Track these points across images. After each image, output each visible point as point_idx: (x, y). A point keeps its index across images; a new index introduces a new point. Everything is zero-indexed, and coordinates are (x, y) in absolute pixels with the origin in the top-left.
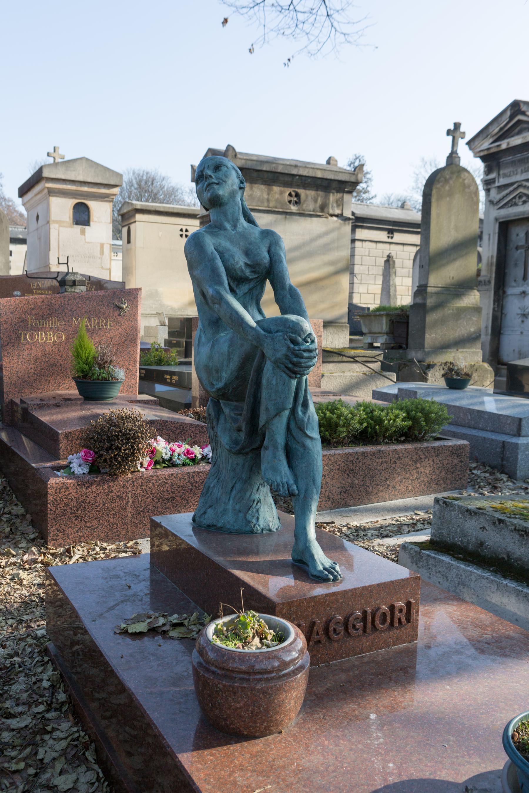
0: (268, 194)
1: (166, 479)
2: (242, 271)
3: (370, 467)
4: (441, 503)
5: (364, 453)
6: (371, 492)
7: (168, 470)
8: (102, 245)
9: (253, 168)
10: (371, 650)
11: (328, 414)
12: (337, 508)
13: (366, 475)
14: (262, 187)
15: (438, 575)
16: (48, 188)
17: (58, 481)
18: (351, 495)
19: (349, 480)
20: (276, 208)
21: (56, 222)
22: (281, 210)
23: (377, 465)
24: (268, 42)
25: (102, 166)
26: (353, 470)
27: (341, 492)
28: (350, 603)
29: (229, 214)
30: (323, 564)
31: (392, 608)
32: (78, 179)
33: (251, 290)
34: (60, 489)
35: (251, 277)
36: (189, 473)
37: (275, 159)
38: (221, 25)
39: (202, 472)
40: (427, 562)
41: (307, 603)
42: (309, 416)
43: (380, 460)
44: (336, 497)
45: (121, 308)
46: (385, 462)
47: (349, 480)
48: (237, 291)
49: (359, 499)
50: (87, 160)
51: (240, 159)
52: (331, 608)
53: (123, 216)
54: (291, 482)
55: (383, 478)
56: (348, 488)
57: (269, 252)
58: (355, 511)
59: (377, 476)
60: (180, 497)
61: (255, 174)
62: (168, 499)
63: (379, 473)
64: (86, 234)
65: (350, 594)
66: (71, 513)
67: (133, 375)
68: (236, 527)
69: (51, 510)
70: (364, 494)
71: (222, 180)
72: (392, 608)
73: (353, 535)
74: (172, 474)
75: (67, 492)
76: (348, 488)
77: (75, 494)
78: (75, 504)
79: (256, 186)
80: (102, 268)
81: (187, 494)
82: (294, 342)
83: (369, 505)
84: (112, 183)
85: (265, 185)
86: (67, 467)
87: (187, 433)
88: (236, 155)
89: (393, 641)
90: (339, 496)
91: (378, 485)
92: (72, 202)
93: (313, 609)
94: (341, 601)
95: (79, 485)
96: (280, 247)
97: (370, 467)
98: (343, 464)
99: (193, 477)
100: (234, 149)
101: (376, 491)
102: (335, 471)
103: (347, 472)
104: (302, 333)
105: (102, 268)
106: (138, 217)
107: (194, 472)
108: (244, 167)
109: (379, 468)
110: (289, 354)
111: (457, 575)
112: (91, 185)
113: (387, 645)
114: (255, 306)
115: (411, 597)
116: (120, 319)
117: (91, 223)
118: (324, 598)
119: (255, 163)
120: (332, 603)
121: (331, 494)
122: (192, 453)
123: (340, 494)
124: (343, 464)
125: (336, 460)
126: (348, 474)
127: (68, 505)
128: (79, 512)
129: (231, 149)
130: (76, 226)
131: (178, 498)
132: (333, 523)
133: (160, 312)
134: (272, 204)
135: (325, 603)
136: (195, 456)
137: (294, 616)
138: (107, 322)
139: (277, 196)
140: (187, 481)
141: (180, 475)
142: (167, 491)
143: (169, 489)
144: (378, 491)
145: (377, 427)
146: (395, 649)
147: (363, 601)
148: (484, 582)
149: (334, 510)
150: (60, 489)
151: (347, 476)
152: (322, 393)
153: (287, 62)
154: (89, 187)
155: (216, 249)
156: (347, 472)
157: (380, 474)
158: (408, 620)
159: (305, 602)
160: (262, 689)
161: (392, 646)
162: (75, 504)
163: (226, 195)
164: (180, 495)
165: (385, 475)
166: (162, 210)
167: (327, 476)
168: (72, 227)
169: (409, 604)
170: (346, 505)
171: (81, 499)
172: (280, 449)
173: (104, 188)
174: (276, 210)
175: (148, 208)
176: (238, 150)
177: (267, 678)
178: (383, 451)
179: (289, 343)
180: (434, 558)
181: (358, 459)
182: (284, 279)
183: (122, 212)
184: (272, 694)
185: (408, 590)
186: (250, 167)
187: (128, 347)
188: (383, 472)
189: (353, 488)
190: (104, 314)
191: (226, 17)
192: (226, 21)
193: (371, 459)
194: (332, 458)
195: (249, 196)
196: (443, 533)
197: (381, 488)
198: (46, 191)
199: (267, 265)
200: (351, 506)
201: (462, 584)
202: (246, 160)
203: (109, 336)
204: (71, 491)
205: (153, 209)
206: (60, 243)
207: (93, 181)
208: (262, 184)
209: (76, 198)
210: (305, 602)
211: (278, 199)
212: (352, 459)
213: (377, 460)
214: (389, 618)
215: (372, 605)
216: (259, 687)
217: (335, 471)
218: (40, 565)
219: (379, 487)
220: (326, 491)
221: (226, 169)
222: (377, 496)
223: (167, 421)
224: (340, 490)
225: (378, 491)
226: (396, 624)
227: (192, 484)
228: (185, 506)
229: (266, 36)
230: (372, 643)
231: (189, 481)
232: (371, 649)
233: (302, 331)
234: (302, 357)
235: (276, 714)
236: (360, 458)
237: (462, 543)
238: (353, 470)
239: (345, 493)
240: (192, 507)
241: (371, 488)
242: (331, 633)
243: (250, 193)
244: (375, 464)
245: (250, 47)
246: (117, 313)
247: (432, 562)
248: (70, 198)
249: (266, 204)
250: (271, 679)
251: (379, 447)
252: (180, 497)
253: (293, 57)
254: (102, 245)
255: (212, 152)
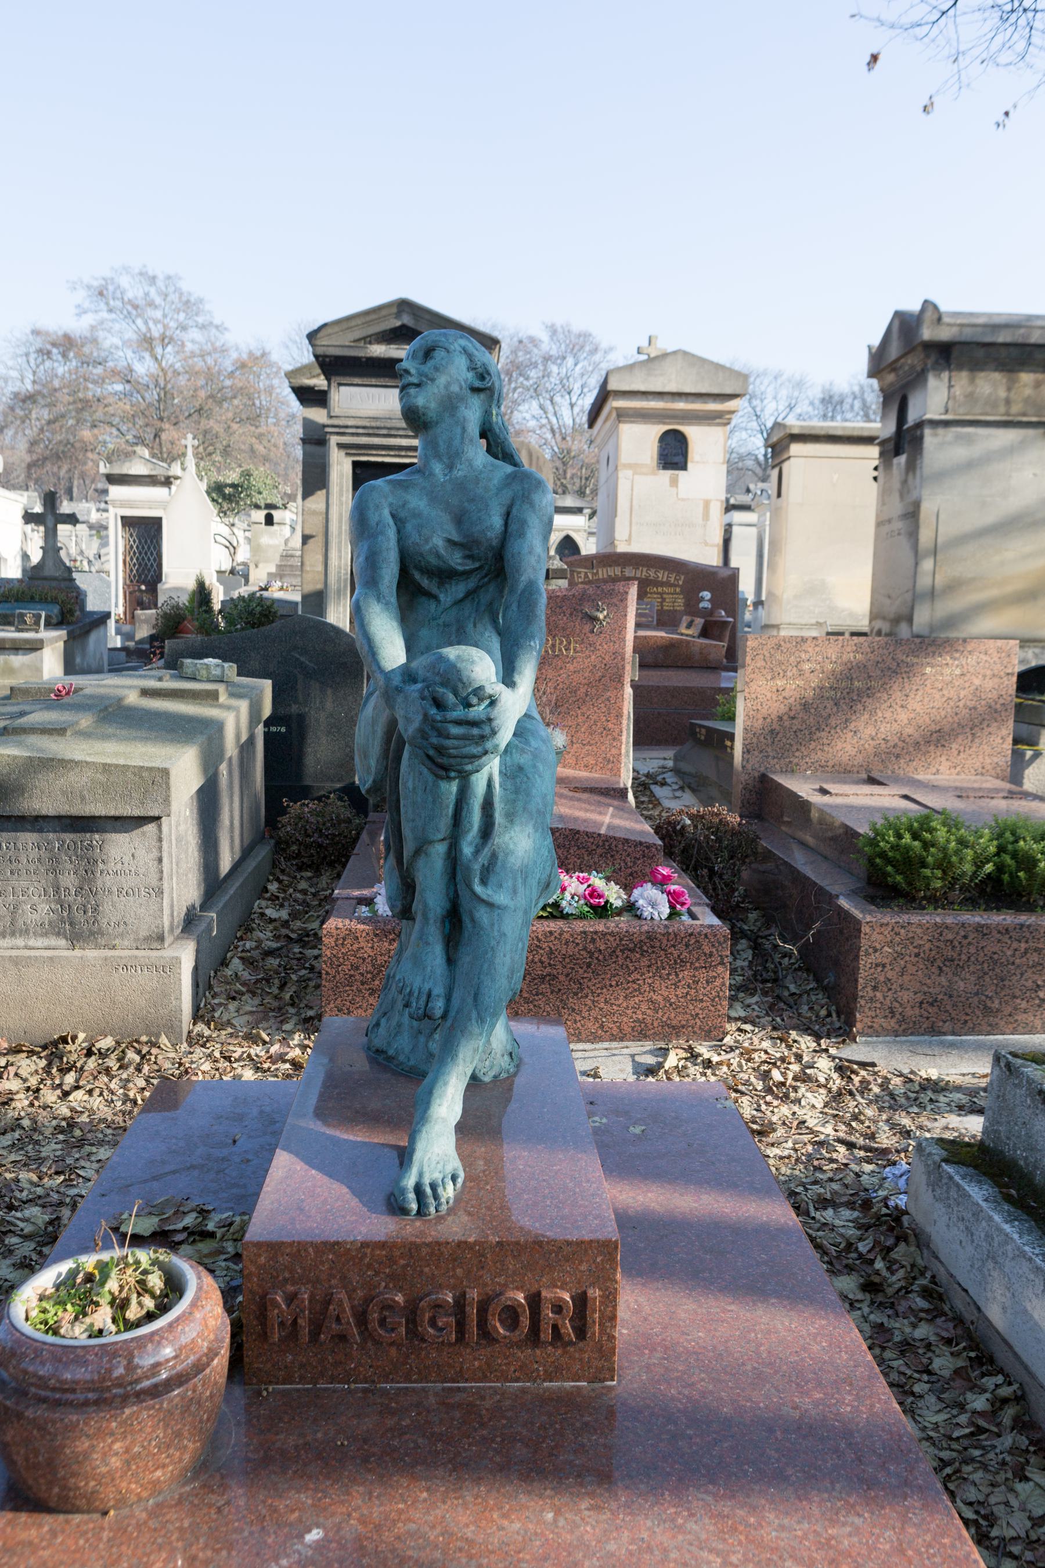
0: (1009, 389)
1: (539, 940)
2: (438, 556)
3: (996, 957)
4: (1002, 1064)
5: (982, 926)
6: (998, 1011)
7: (546, 923)
8: (707, 504)
9: (975, 339)
10: (484, 1378)
11: (907, 839)
12: (912, 1034)
13: (985, 974)
14: (997, 376)
15: (960, 1224)
16: (617, 409)
17: (340, 925)
18: (947, 1011)
19: (945, 982)
20: (1024, 415)
21: (629, 466)
22: (1034, 419)
23: (1014, 955)
24: (968, 85)
25: (712, 363)
26: (953, 961)
27: (921, 1003)
28: (426, 1270)
29: (441, 443)
30: (421, 1175)
31: (535, 1300)
32: (667, 389)
33: (469, 594)
34: (344, 939)
35: (460, 568)
36: (585, 932)
37: (1030, 318)
38: (866, 68)
39: (612, 934)
40: (947, 1192)
41: (316, 1253)
42: (494, 856)
43: (1023, 945)
44: (909, 1012)
45: (595, 619)
46: (1035, 950)
47: (943, 980)
48: (442, 597)
49: (966, 1022)
50: (685, 353)
51: (949, 325)
52: (377, 1274)
53: (773, 447)
54: (439, 990)
55: (1029, 984)
56: (940, 997)
57: (507, 515)
58: (952, 1045)
59: (1015, 978)
60: (567, 975)
61: (980, 353)
62: (543, 978)
63: (1018, 972)
64: (680, 485)
65: (424, 1251)
66: (363, 983)
67: (614, 739)
68: (412, 1063)
69: (327, 973)
70: (978, 1013)
71: (426, 376)
72: (535, 1300)
73: (908, 1098)
74: (551, 933)
75: (356, 946)
76: (940, 997)
77: (369, 951)
78: (370, 968)
79: (982, 374)
80: (706, 544)
81: (581, 971)
82: (439, 704)
83: (992, 1037)
84: (728, 391)
85: (1002, 371)
86: (369, 902)
87: (617, 856)
88: (939, 319)
89: (545, 1371)
90: (917, 1011)
91: (1015, 997)
92: (657, 430)
93: (331, 1268)
94: (402, 1262)
95: (376, 935)
96: (532, 505)
97: (996, 957)
98: (928, 946)
99: (593, 941)
100: (935, 307)
101: (1010, 1009)
102: (907, 958)
103: (939, 963)
104: (460, 685)
105: (706, 544)
106: (795, 448)
107: (596, 933)
108: (958, 339)
109: (1018, 961)
110: (427, 729)
111: (987, 1236)
112: (690, 398)
113: (526, 1372)
114: (489, 627)
115: (593, 1284)
116: (592, 638)
117: (690, 465)
118: (358, 1250)
119: (979, 329)
120: (380, 1263)
121: (897, 1005)
122: (600, 896)
123: (920, 1007)
124: (928, 946)
125: (911, 935)
126: (940, 968)
127: (357, 968)
128: (377, 982)
129: (930, 308)
130: (662, 472)
131: (562, 978)
132: (873, 1065)
133: (821, 621)
134: (1015, 409)
135: (361, 1259)
136: (607, 902)
137: (287, 1275)
138: (569, 643)
139: (1028, 392)
140: (581, 947)
141: (566, 936)
142: (542, 962)
143: (545, 959)
144: (1016, 1009)
145: (1021, 874)
146: (548, 1389)
147: (459, 1271)
148: (1026, 1266)
149: (904, 1038)
150: (344, 939)
151: (937, 972)
152: (1021, 793)
153: (1001, 117)
154: (687, 402)
155: (393, 516)
156: (939, 963)
157: (1022, 974)
158: (581, 1332)
159: (311, 1250)
160: (34, 1419)
161: (544, 1380)
162: (370, 968)
163: (433, 405)
164: (565, 971)
165: (1036, 977)
166: (839, 433)
167: (888, 967)
168: (654, 474)
169: (581, 1301)
170: (934, 1031)
171: (380, 960)
172: (431, 921)
173: (715, 401)
174: (1025, 419)
175: (813, 432)
176: (943, 308)
177: (60, 1400)
178: (1029, 926)
179: (427, 704)
180: (958, 1186)
181: (965, 937)
182: (517, 571)
183: (770, 442)
184: (56, 1435)
185: (583, 1267)
186: (968, 339)
187: (606, 689)
188: (1030, 971)
189: (951, 996)
190: (564, 629)
191: (875, 52)
192: (875, 58)
193: (999, 941)
194: (902, 931)
195: (966, 396)
196: (999, 1132)
197: (1024, 1005)
198: (614, 415)
199: (495, 543)
200: (945, 1034)
201: (993, 1258)
202: (962, 325)
203: (572, 668)
204: (362, 944)
205: (823, 433)
206: (635, 502)
207: (693, 391)
208: (996, 370)
209: (664, 423)
210: (311, 1250)
211: (1029, 397)
212: (950, 937)
213: (1015, 945)
214: (525, 1321)
215: (486, 1285)
216: (29, 1413)
217: (907, 958)
218: (287, 1066)
219: (1018, 1001)
220: (885, 997)
221: (443, 353)
222: (1011, 1019)
223: (578, 832)
224: (920, 997)
225: (1016, 1009)
226: (546, 1335)
227: (591, 954)
228: (576, 994)
229: (963, 73)
230: (488, 1364)
231: (585, 949)
232: (485, 1376)
233: (461, 680)
234: (448, 737)
235: (74, 1475)
236: (971, 936)
237: (1027, 1165)
238: (953, 961)
239: (932, 1004)
240: (590, 997)
241: (997, 1002)
242: (374, 1324)
243: (969, 389)
244: (1009, 953)
245: (925, 101)
246: (587, 628)
247: (953, 1193)
248: (654, 423)
249: (1002, 409)
250: (65, 1405)
251: (1023, 918)
252: (567, 975)
253: (1015, 107)
254: (707, 504)
255: (900, 317)
